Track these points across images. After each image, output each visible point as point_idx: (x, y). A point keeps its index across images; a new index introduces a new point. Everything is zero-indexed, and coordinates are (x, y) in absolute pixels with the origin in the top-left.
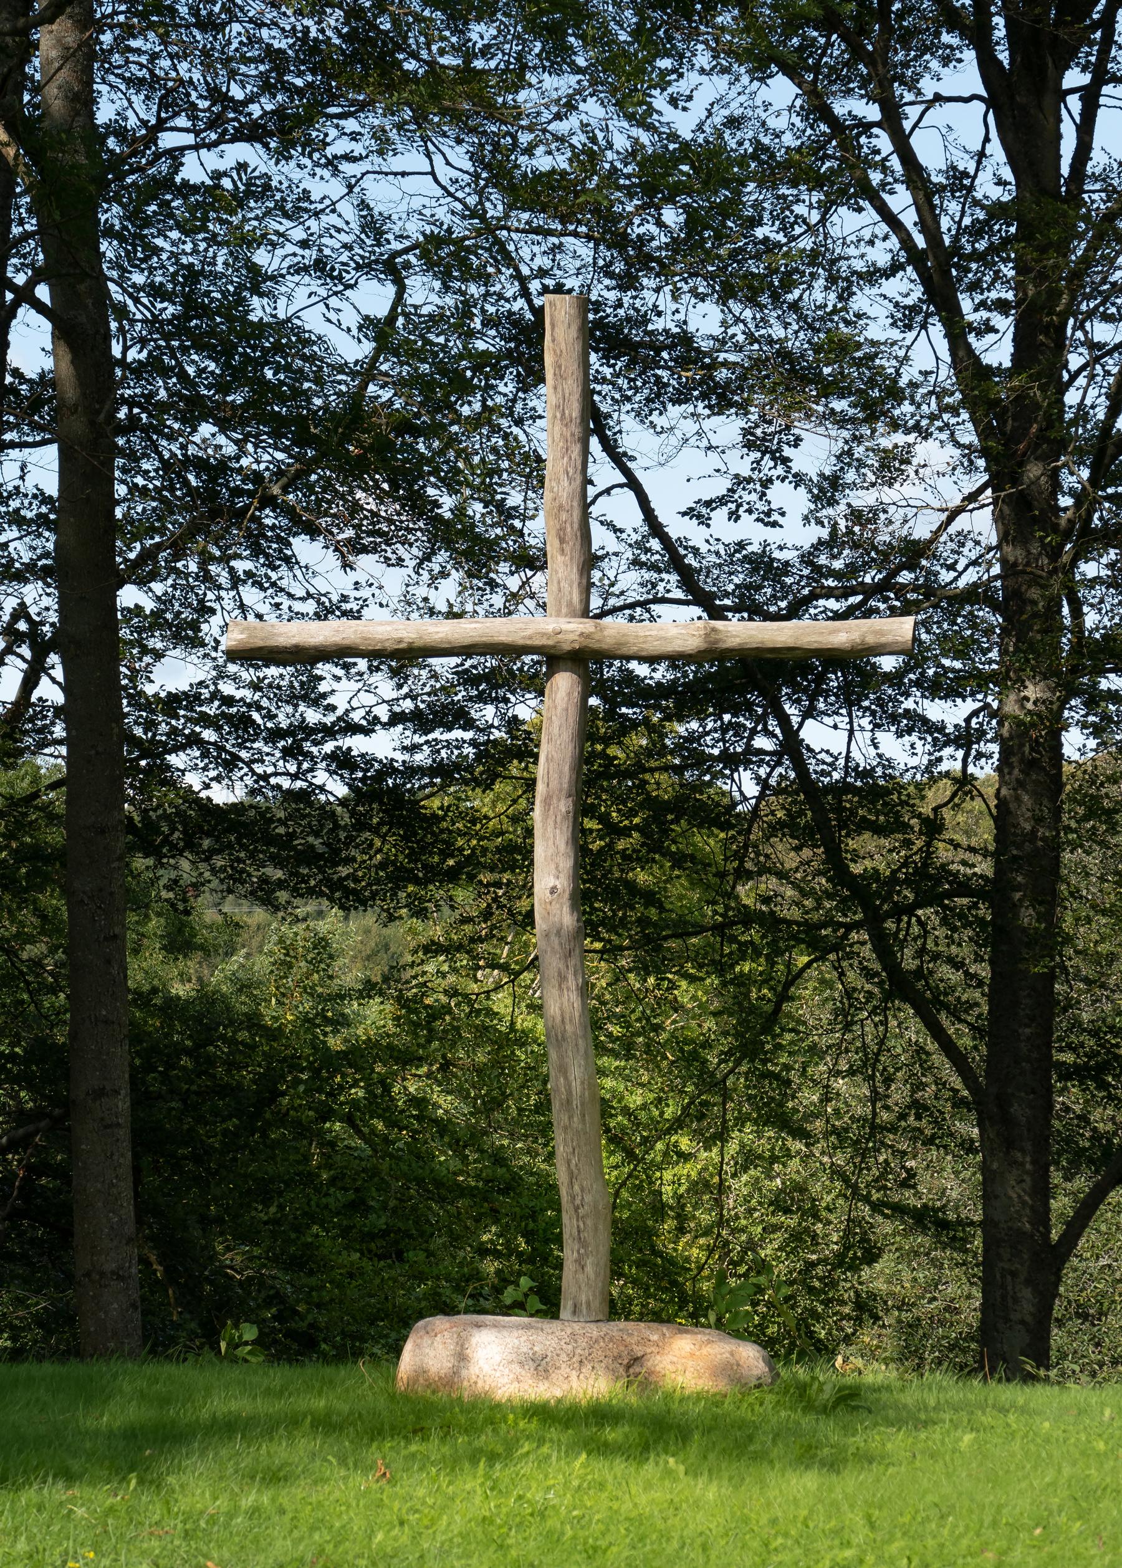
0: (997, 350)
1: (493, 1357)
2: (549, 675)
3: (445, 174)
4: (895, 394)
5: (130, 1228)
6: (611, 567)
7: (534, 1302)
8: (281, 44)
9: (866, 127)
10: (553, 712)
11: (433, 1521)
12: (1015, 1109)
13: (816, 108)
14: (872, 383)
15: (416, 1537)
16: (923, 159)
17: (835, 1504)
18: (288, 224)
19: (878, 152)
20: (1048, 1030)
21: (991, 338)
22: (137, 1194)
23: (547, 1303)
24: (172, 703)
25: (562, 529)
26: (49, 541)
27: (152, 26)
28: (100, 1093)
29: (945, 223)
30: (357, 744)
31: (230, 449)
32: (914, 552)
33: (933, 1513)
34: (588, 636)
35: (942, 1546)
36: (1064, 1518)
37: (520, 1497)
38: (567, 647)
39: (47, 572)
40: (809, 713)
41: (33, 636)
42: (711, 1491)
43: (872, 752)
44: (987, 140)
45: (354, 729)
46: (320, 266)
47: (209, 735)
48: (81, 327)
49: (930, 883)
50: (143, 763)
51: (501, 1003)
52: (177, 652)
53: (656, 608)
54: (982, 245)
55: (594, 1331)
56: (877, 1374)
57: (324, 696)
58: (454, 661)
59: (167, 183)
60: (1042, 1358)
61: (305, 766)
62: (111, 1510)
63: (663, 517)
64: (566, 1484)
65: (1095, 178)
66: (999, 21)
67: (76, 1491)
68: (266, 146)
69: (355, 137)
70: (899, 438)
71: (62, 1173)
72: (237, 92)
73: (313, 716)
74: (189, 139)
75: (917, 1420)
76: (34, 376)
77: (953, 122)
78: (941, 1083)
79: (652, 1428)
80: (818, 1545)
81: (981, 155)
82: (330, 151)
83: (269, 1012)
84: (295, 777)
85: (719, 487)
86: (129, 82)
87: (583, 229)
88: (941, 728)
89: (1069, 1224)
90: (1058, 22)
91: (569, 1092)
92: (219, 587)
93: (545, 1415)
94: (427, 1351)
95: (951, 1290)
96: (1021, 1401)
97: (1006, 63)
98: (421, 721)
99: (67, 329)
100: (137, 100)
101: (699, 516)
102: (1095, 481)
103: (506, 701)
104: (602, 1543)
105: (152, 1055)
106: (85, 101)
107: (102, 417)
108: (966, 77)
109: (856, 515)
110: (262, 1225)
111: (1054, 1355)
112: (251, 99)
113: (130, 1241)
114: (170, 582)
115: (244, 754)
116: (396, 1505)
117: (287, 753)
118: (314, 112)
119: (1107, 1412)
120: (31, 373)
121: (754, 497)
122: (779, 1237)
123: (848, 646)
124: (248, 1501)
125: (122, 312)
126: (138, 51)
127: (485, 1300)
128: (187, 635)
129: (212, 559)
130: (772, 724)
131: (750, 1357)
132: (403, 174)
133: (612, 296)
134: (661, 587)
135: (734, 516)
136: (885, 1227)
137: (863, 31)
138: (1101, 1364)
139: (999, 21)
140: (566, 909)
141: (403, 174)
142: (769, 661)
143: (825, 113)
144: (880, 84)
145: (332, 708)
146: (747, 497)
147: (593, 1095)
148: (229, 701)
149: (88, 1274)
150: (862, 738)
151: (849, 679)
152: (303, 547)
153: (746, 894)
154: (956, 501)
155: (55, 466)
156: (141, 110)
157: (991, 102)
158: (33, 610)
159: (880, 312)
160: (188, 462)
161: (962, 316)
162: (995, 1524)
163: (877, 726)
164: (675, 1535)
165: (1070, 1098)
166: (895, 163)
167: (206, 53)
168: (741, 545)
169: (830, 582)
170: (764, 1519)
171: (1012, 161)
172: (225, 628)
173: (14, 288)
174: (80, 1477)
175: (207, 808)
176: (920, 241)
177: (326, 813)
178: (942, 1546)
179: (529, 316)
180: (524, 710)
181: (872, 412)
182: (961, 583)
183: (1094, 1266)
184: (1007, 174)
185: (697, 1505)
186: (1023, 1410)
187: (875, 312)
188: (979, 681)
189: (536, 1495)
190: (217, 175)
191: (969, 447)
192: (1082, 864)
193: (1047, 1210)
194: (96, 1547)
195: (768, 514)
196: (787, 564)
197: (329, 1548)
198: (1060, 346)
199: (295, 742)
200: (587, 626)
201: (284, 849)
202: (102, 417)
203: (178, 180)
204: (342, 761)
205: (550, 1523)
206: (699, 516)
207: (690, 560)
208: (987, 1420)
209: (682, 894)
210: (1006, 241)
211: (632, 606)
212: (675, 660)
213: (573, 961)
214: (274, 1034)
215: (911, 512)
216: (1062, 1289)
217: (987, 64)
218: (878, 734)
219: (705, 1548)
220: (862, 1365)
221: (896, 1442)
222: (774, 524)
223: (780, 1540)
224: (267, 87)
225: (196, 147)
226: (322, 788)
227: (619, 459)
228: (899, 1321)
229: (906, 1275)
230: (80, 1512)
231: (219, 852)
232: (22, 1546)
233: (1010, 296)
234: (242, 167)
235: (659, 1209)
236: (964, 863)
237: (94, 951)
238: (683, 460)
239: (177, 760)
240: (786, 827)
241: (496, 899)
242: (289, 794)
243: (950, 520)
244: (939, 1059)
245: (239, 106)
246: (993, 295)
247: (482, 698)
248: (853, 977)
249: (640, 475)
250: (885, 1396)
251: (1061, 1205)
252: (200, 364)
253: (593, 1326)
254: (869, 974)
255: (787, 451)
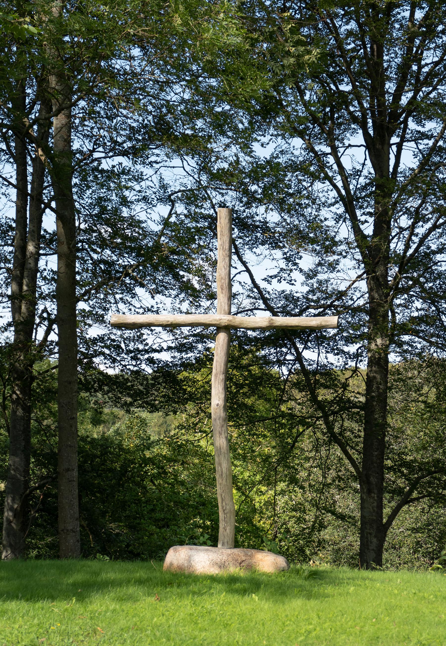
0: (368, 229)
1: (201, 560)
2: (216, 334)
3: (188, 168)
4: (335, 244)
5: (77, 515)
6: (240, 298)
7: (209, 542)
8: (135, 125)
9: (326, 154)
10: (219, 346)
11: (174, 614)
12: (372, 479)
13: (310, 148)
14: (327, 239)
15: (167, 620)
16: (344, 165)
17: (307, 610)
18: (135, 183)
19: (329, 163)
20: (382, 453)
21: (366, 225)
22: (80, 504)
23: (214, 541)
24: (94, 341)
25: (222, 285)
26: (53, 286)
27: (92, 118)
28: (68, 470)
29: (351, 187)
30: (156, 356)
31: (115, 258)
32: (341, 295)
33: (340, 613)
34: (230, 321)
35: (342, 625)
36: (383, 616)
37: (203, 607)
38: (223, 324)
39: (54, 297)
40: (306, 348)
41: (49, 319)
42: (266, 605)
43: (326, 360)
44: (366, 159)
45: (155, 351)
46: (145, 199)
47: (107, 351)
48: (66, 216)
49: (345, 405)
50: (85, 360)
51: (203, 443)
52: (97, 325)
53: (255, 311)
54: (363, 194)
55: (229, 551)
56: (325, 567)
57: (144, 340)
58: (189, 328)
59: (96, 169)
60: (379, 562)
61: (138, 363)
62: (66, 610)
63: (257, 282)
64: (218, 603)
65: (401, 173)
66: (370, 121)
67: (55, 603)
68: (129, 158)
69: (158, 155)
70: (336, 257)
71: (56, 496)
72: (119, 140)
73: (141, 347)
74: (103, 155)
75: (336, 582)
76: (52, 232)
77: (355, 154)
78: (347, 470)
79: (253, 584)
80: (301, 624)
81: (364, 164)
82: (150, 160)
83: (125, 444)
84: (135, 366)
85: (275, 272)
86: (84, 136)
87: (233, 188)
88: (348, 353)
89: (389, 517)
90: (389, 122)
91: (222, 472)
92: (111, 303)
93: (213, 579)
94: (176, 556)
95: (351, 539)
96: (370, 576)
97: (372, 134)
98: (181, 348)
99: (60, 218)
100: (87, 142)
101: (268, 281)
102: (400, 272)
103: (205, 342)
104: (229, 622)
105: (86, 457)
106: (69, 141)
107: (71, 246)
108: (358, 138)
109: (320, 282)
110: (111, 516)
111: (384, 561)
112: (124, 142)
113: (77, 519)
114: (94, 301)
115: (118, 358)
116: (161, 609)
117: (132, 358)
118: (145, 147)
119: (399, 580)
120: (50, 231)
121: (286, 275)
122: (293, 520)
123: (316, 325)
124: (111, 608)
125: (79, 212)
126: (87, 126)
127: (193, 541)
128: (100, 319)
129: (109, 294)
130: (293, 351)
131: (281, 561)
132: (173, 167)
133: (242, 209)
134: (257, 304)
135: (279, 281)
136: (329, 517)
137: (325, 123)
138: (400, 564)
139: (370, 121)
140: (222, 411)
141: (173, 167)
142: (289, 330)
143: (312, 150)
144: (331, 141)
145: (147, 344)
146: (284, 275)
147: (230, 474)
148: (114, 341)
149: (63, 530)
150: (323, 356)
151: (316, 336)
152: (139, 290)
153: (283, 408)
154: (354, 279)
155: (57, 262)
156: (88, 146)
157: (367, 147)
158: (49, 310)
159: (329, 216)
160: (102, 261)
161: (357, 217)
162: (360, 617)
163: (327, 352)
164: (254, 620)
165: (390, 476)
166: (335, 167)
167: (109, 127)
168: (283, 291)
169: (313, 304)
170: (283, 615)
171: (374, 167)
172: (111, 317)
173: (44, 203)
174: (56, 598)
175: (106, 376)
176: (343, 192)
177: (145, 378)
178: (342, 625)
179: (214, 215)
180: (211, 345)
181: (328, 250)
182: (355, 305)
183: (398, 531)
184: (372, 171)
185: (261, 610)
186: (371, 580)
187: (327, 215)
188: (361, 337)
189: (208, 606)
190: (114, 166)
191: (358, 260)
192: (395, 399)
193: (382, 513)
194: (61, 622)
195: (291, 281)
196: (298, 298)
197: (138, 623)
198: (389, 229)
199: (135, 355)
200: (230, 317)
201: (131, 390)
202: (71, 246)
203: (100, 168)
204: (151, 361)
205: (212, 615)
206: (268, 281)
207: (267, 296)
208: (359, 582)
209: (261, 406)
210: (372, 193)
211: (247, 311)
212: (262, 330)
213: (224, 428)
214: (128, 451)
215: (339, 282)
216: (387, 539)
217: (366, 135)
218: (328, 354)
219: (263, 625)
220: (320, 563)
221: (329, 590)
222: (293, 284)
223: (288, 622)
224: (130, 139)
225: (104, 158)
226: (144, 370)
227: (244, 264)
228: (333, 549)
229: (336, 534)
230: (56, 610)
231: (111, 392)
232: (36, 621)
233: (372, 211)
234: (120, 164)
235: (254, 510)
236: (355, 397)
237: (67, 422)
238: (264, 262)
239: (96, 360)
240: (296, 385)
241: (200, 408)
242: (132, 371)
243: (353, 284)
244: (347, 461)
245: (120, 144)
246: (368, 210)
247: (197, 342)
248: (319, 435)
249: (250, 268)
250: (325, 574)
251: (387, 511)
252: (105, 230)
253: (229, 550)
254: (324, 434)
255: (297, 261)
